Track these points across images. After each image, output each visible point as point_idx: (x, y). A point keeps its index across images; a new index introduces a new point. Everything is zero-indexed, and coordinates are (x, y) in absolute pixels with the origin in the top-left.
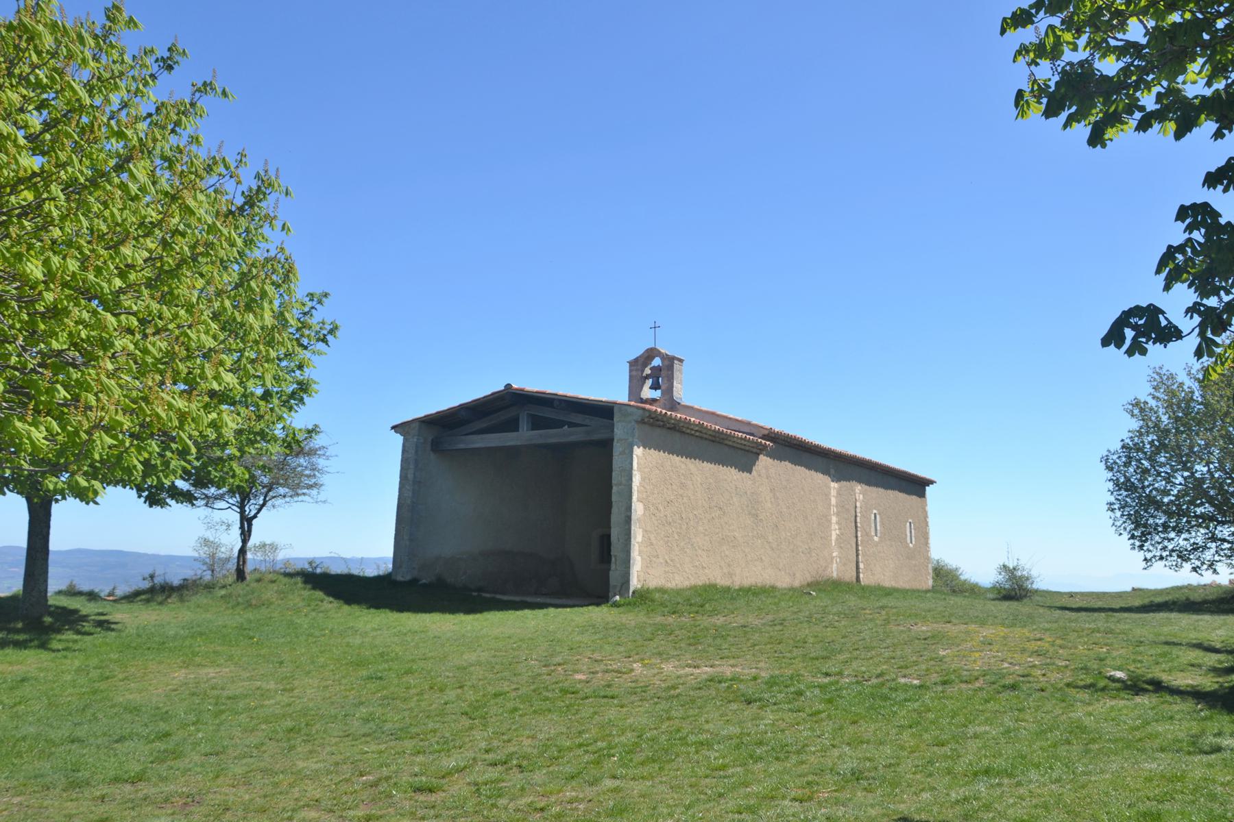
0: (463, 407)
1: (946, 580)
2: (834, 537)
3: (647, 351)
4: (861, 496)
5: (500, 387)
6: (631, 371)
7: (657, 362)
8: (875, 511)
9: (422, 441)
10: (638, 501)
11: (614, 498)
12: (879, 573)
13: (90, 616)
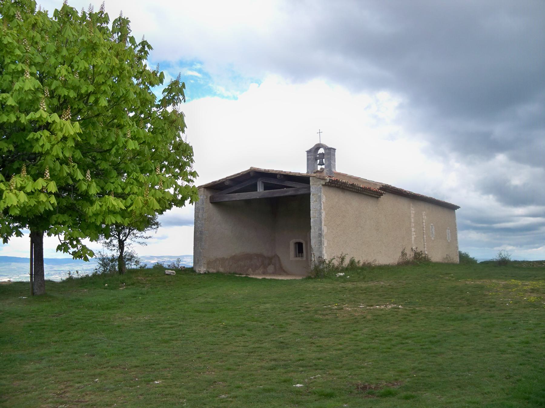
0: (227, 179)
1: (465, 259)
2: (413, 239)
3: (316, 145)
4: (425, 217)
5: (249, 168)
6: (308, 156)
7: (321, 151)
8: (432, 224)
9: (205, 198)
10: (324, 225)
11: (312, 225)
12: (436, 256)
13: (302, 280)
